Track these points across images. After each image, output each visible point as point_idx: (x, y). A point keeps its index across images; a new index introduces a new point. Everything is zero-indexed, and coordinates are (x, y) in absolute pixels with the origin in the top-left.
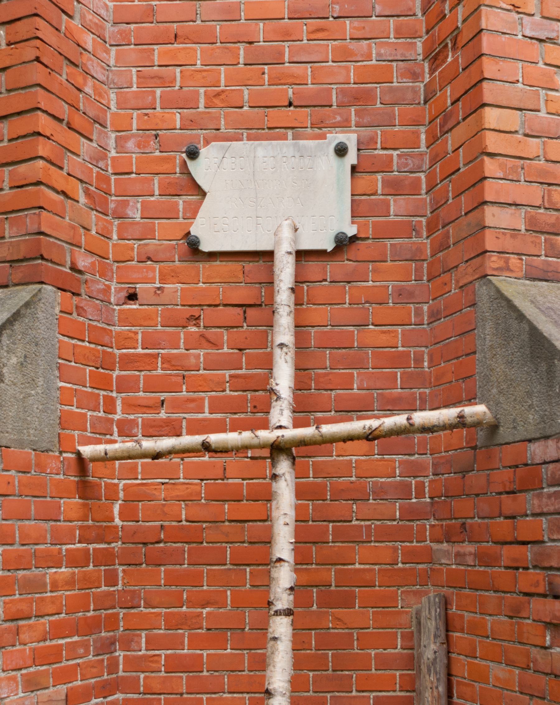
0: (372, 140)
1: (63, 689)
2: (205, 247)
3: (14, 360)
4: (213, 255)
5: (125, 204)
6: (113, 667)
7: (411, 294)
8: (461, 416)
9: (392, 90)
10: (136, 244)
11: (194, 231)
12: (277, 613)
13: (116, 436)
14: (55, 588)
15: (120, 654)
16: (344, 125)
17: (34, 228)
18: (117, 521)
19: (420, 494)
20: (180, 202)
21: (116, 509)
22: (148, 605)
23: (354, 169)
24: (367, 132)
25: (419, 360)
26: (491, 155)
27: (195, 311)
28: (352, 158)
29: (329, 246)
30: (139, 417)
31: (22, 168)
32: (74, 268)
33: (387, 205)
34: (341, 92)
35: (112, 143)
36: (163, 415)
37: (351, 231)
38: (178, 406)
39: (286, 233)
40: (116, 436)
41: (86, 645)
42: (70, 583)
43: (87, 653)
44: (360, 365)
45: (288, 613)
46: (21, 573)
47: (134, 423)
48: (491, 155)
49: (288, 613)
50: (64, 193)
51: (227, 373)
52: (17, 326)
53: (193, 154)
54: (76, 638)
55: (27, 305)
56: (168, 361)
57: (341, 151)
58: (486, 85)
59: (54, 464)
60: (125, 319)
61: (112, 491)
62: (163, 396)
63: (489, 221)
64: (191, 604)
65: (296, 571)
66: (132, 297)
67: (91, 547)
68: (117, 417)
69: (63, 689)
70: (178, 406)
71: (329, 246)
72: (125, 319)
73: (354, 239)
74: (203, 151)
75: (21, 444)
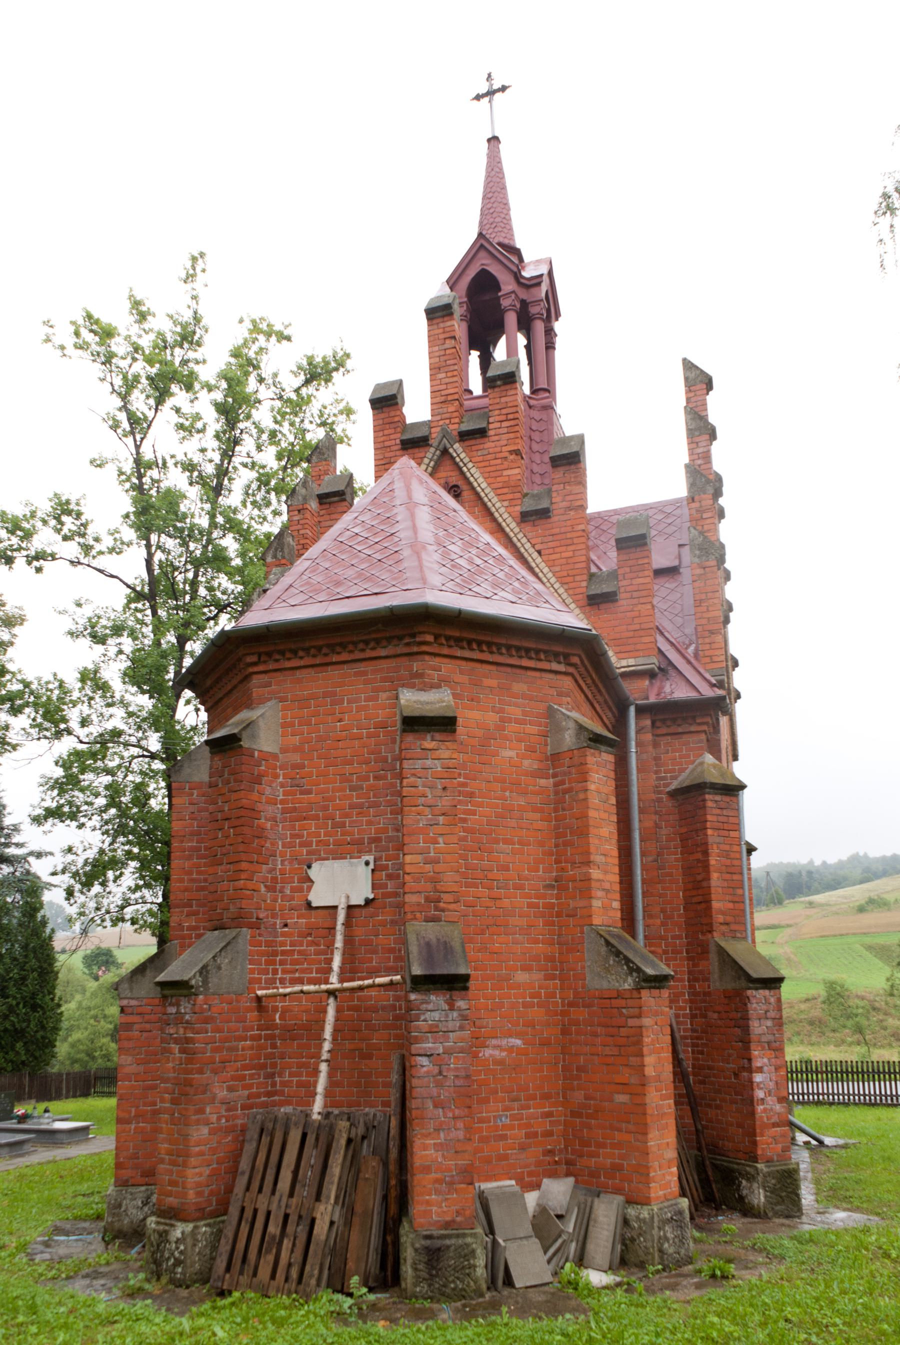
0: (381, 858)
1: (246, 1092)
2: (314, 904)
3: (227, 961)
4: (317, 908)
5: (284, 887)
6: (274, 1084)
7: (396, 922)
8: (391, 981)
9: (389, 837)
10: (288, 904)
11: (310, 898)
12: (322, 1061)
13: (278, 984)
14: (243, 1049)
15: (277, 1079)
16: (370, 851)
17: (239, 906)
18: (278, 1021)
19: (400, 1009)
20: (305, 885)
21: (277, 1016)
22: (289, 1058)
23: (373, 870)
24: (378, 854)
25: (400, 951)
26: (408, 874)
27: (310, 931)
28: (372, 866)
29: (362, 903)
30: (288, 976)
31: (236, 883)
32: (258, 918)
33: (387, 884)
34: (369, 838)
35: (279, 862)
36: (297, 975)
37: (371, 896)
38: (303, 971)
39: (343, 900)
40: (278, 984)
41: (259, 1075)
42: (251, 1048)
43: (259, 1078)
44: (375, 952)
45: (327, 1061)
46: (227, 1044)
47: (285, 979)
48: (408, 874)
49: (327, 1061)
50: (254, 890)
51: (323, 957)
52: (229, 948)
53: (309, 867)
54: (254, 1071)
55: (234, 938)
56: (300, 952)
57: (367, 863)
58: (405, 847)
59: (245, 1000)
60: (283, 935)
61: (275, 1009)
62: (297, 967)
63: (407, 900)
64: (307, 1057)
65: (333, 1043)
66: (286, 925)
67: (263, 1033)
68: (279, 976)
69: (246, 1092)
70: (303, 971)
71: (362, 903)
72: (283, 935)
73: (373, 899)
74: (313, 865)
75: (229, 993)
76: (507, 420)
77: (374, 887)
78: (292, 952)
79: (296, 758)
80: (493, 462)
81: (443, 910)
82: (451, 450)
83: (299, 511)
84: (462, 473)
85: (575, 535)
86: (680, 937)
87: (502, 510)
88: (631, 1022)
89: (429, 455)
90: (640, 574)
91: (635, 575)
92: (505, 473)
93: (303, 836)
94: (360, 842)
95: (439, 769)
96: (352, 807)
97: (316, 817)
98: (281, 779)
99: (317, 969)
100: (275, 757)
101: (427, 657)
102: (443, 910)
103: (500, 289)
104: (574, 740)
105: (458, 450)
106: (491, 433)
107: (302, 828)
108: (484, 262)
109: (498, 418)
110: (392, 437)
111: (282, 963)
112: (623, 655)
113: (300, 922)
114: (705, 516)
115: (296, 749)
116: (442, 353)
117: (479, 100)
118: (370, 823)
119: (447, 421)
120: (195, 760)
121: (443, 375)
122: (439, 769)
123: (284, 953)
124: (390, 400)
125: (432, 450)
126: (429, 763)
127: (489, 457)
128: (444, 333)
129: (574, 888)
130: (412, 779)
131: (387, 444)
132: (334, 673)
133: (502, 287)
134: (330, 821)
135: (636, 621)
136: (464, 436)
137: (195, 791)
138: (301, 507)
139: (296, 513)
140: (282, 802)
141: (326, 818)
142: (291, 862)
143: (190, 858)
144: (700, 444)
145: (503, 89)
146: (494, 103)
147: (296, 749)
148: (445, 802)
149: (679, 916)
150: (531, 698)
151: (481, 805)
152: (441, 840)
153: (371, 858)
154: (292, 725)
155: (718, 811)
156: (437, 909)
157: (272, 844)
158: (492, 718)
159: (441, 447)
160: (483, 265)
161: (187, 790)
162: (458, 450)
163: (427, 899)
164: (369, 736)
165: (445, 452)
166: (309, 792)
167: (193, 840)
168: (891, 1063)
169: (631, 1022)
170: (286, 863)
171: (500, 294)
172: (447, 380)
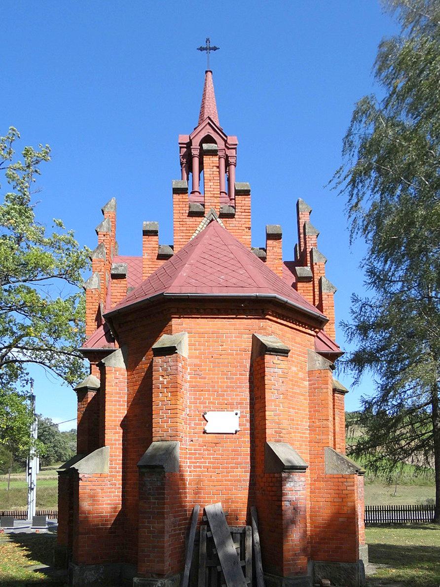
10: (192, 430)
24: (242, 410)
28: (239, 415)
29: (234, 432)
36: (198, 464)
38: (202, 463)
57: (236, 414)
70: (202, 463)
76: (245, 212)
77: (240, 425)
78: (195, 454)
79: (197, 361)
80: (237, 231)
83: (104, 235)
85: (277, 272)
88: (349, 488)
91: (305, 294)
92: (243, 237)
93: (201, 399)
94: (232, 404)
95: (281, 373)
96: (228, 387)
97: (209, 391)
98: (189, 370)
99: (208, 462)
101: (267, 321)
104: (321, 365)
106: (235, 217)
107: (200, 395)
109: (240, 210)
110: (184, 209)
111: (190, 458)
114: (321, 272)
115: (196, 357)
116: (212, 173)
117: (201, 50)
118: (237, 395)
119: (214, 207)
120: (118, 357)
121: (212, 184)
122: (281, 373)
124: (184, 190)
125: (205, 219)
127: (235, 228)
128: (213, 163)
129: (319, 431)
130: (270, 377)
131: (181, 212)
134: (216, 393)
136: (222, 216)
137: (117, 372)
138: (105, 233)
139: (103, 236)
140: (189, 382)
142: (195, 411)
143: (115, 405)
144: (312, 239)
145: (215, 49)
148: (283, 389)
149: (119, 444)
152: (281, 405)
153: (239, 412)
154: (195, 345)
155: (339, 401)
156: (280, 436)
160: (208, 132)
161: (113, 371)
163: (276, 432)
164: (237, 354)
166: (205, 378)
167: (116, 397)
168: (424, 506)
169: (349, 488)
170: (192, 411)
171: (192, 147)
172: (214, 187)
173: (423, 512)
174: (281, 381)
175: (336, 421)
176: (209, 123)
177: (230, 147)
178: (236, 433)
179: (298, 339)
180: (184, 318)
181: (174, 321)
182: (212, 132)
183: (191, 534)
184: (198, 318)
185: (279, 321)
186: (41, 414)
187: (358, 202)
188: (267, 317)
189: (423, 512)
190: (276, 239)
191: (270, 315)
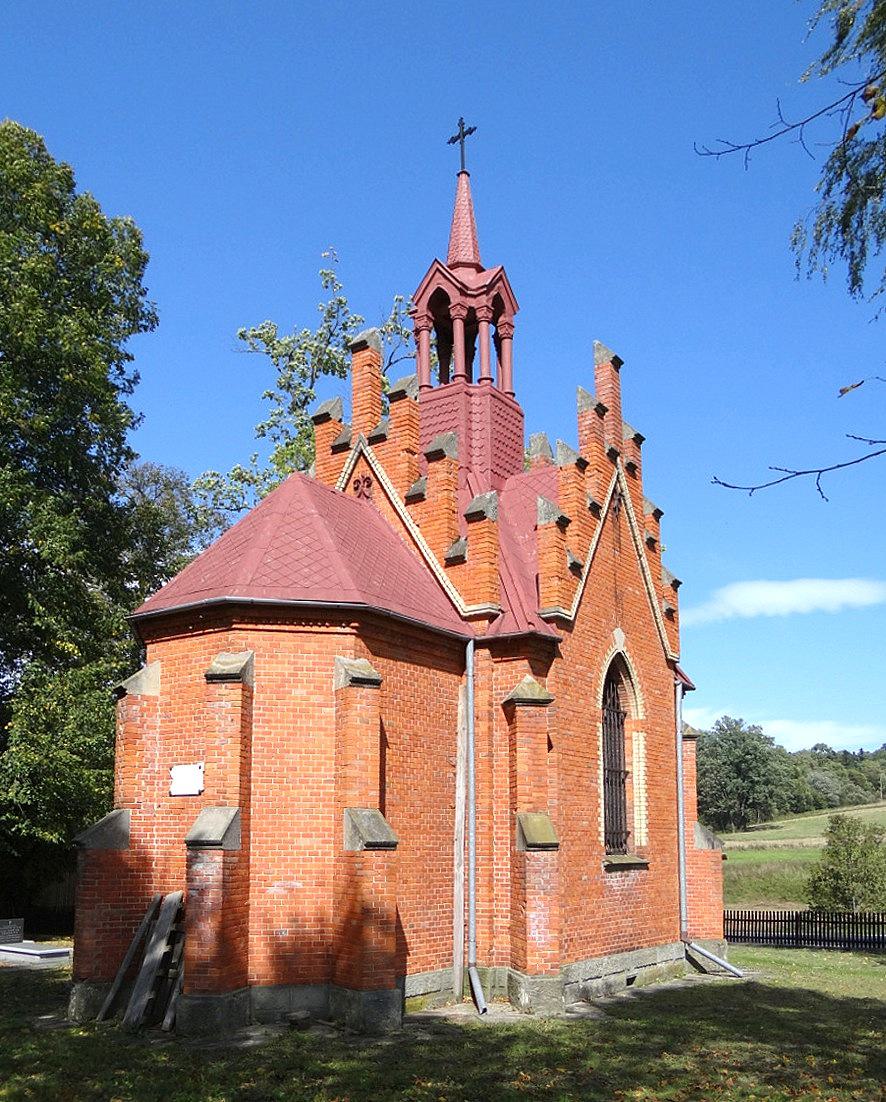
28: (202, 769)
29: (197, 793)
81: (228, 799)
82: (364, 452)
84: (372, 469)
86: (329, 818)
87: (396, 495)
89: (351, 456)
90: (482, 540)
100: (156, 698)
102: (228, 799)
103: (449, 303)
105: (369, 451)
108: (440, 281)
112: (469, 602)
113: (166, 804)
115: (169, 693)
123: (158, 824)
125: (352, 452)
126: (223, 703)
132: (188, 642)
133: (452, 300)
135: (478, 576)
141: (181, 737)
146: (466, 143)
147: (169, 693)
150: (321, 653)
151: (276, 728)
152: (229, 753)
157: (151, 755)
158: (287, 669)
159: (359, 450)
162: (369, 451)
165: (361, 453)
173: (879, 936)
174: (230, 719)
175: (518, 755)
176: (438, 269)
177: (475, 293)
178: (200, 794)
179: (308, 646)
180: (158, 642)
181: (150, 648)
182: (444, 280)
183: (823, 957)
184: (169, 640)
185: (261, 627)
186: (741, 720)
187: (863, 244)
188: (234, 626)
189: (879, 936)
190: (438, 459)
191: (236, 623)
